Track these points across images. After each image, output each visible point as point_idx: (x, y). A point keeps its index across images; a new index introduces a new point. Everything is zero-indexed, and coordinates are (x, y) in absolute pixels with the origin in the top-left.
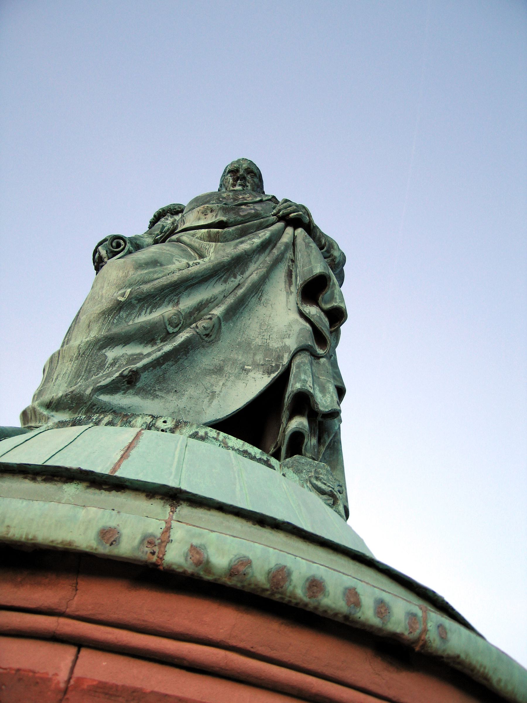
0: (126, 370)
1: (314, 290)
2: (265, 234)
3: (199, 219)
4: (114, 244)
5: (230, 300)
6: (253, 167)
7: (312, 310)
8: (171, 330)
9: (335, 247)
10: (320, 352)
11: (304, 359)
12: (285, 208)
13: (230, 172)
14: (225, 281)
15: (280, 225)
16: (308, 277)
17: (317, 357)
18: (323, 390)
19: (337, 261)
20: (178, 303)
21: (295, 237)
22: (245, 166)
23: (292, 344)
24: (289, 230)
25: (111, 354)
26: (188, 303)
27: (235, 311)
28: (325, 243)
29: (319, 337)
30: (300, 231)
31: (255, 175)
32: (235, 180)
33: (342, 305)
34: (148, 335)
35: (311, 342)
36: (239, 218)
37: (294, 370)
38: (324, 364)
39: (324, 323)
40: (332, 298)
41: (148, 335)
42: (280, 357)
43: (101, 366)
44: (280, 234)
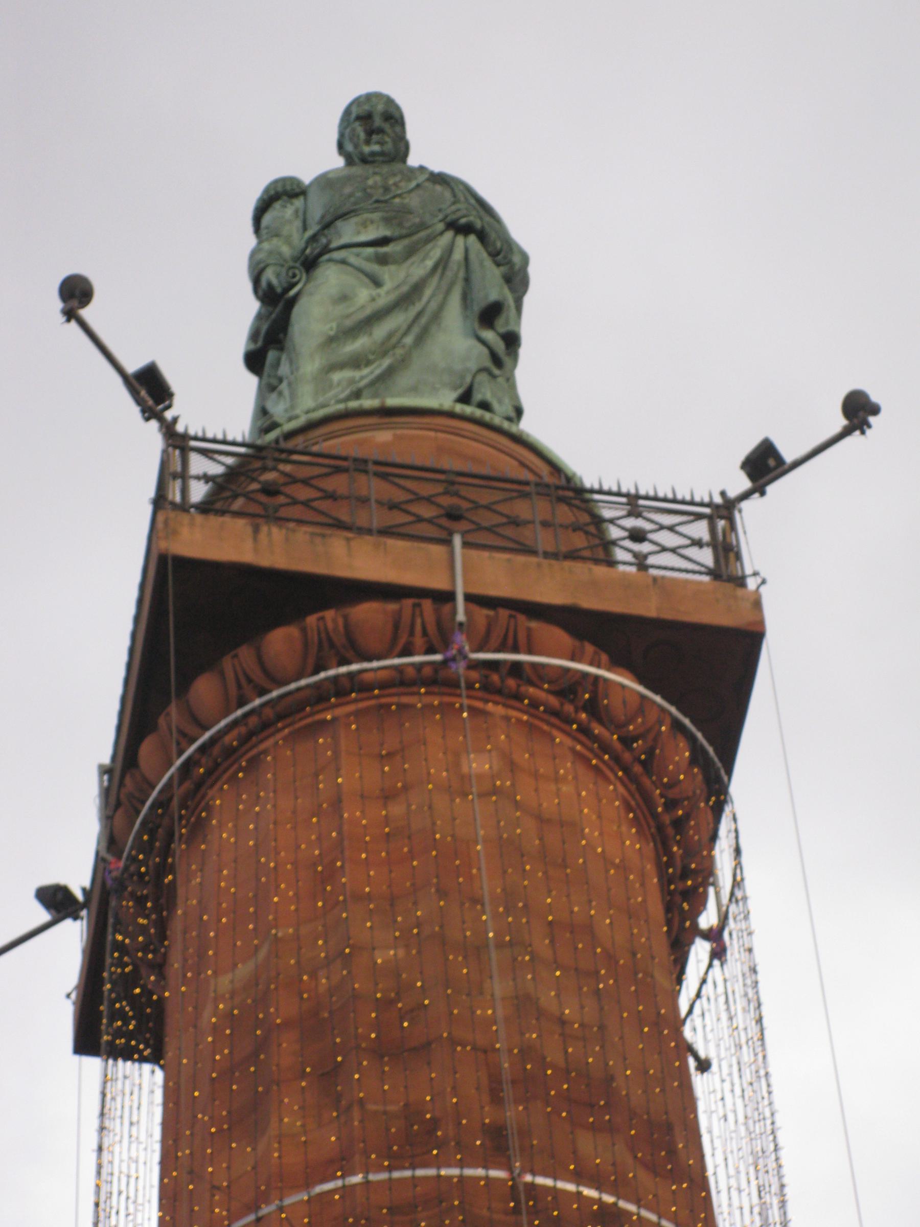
0: (354, 388)
1: (490, 315)
2: (436, 253)
3: (359, 233)
4: (290, 274)
5: (416, 330)
6: (392, 110)
7: (489, 335)
8: (371, 357)
9: (515, 249)
10: (496, 372)
11: (483, 377)
12: (454, 212)
13: (358, 118)
14: (406, 309)
15: (449, 235)
16: (483, 304)
17: (494, 377)
18: (500, 402)
19: (517, 267)
20: (371, 334)
21: (467, 251)
22: (380, 107)
23: (473, 365)
24: (460, 240)
25: (337, 376)
26: (380, 331)
27: (420, 340)
28: (502, 245)
29: (497, 360)
30: (472, 238)
31: (397, 121)
32: (370, 133)
33: (516, 329)
34: (356, 362)
35: (488, 363)
36: (404, 232)
37: (476, 386)
38: (561, 742)
39: (500, 346)
40: (507, 322)
41: (356, 362)
42: (462, 377)
43: (331, 387)
44: (450, 250)
